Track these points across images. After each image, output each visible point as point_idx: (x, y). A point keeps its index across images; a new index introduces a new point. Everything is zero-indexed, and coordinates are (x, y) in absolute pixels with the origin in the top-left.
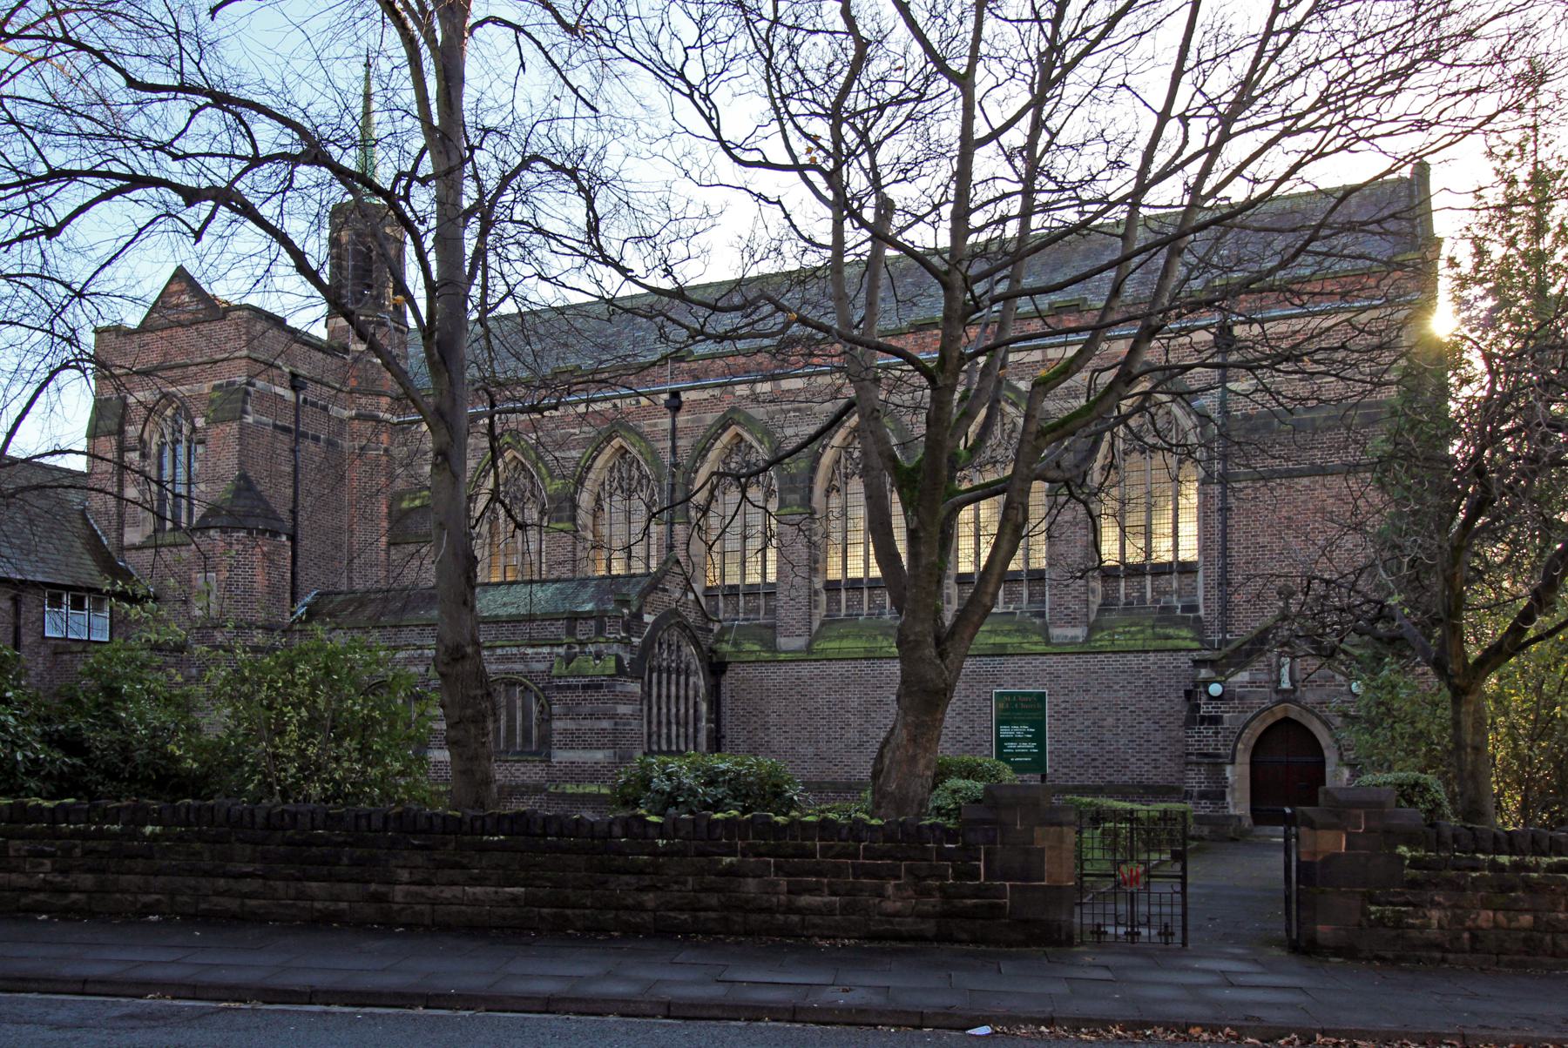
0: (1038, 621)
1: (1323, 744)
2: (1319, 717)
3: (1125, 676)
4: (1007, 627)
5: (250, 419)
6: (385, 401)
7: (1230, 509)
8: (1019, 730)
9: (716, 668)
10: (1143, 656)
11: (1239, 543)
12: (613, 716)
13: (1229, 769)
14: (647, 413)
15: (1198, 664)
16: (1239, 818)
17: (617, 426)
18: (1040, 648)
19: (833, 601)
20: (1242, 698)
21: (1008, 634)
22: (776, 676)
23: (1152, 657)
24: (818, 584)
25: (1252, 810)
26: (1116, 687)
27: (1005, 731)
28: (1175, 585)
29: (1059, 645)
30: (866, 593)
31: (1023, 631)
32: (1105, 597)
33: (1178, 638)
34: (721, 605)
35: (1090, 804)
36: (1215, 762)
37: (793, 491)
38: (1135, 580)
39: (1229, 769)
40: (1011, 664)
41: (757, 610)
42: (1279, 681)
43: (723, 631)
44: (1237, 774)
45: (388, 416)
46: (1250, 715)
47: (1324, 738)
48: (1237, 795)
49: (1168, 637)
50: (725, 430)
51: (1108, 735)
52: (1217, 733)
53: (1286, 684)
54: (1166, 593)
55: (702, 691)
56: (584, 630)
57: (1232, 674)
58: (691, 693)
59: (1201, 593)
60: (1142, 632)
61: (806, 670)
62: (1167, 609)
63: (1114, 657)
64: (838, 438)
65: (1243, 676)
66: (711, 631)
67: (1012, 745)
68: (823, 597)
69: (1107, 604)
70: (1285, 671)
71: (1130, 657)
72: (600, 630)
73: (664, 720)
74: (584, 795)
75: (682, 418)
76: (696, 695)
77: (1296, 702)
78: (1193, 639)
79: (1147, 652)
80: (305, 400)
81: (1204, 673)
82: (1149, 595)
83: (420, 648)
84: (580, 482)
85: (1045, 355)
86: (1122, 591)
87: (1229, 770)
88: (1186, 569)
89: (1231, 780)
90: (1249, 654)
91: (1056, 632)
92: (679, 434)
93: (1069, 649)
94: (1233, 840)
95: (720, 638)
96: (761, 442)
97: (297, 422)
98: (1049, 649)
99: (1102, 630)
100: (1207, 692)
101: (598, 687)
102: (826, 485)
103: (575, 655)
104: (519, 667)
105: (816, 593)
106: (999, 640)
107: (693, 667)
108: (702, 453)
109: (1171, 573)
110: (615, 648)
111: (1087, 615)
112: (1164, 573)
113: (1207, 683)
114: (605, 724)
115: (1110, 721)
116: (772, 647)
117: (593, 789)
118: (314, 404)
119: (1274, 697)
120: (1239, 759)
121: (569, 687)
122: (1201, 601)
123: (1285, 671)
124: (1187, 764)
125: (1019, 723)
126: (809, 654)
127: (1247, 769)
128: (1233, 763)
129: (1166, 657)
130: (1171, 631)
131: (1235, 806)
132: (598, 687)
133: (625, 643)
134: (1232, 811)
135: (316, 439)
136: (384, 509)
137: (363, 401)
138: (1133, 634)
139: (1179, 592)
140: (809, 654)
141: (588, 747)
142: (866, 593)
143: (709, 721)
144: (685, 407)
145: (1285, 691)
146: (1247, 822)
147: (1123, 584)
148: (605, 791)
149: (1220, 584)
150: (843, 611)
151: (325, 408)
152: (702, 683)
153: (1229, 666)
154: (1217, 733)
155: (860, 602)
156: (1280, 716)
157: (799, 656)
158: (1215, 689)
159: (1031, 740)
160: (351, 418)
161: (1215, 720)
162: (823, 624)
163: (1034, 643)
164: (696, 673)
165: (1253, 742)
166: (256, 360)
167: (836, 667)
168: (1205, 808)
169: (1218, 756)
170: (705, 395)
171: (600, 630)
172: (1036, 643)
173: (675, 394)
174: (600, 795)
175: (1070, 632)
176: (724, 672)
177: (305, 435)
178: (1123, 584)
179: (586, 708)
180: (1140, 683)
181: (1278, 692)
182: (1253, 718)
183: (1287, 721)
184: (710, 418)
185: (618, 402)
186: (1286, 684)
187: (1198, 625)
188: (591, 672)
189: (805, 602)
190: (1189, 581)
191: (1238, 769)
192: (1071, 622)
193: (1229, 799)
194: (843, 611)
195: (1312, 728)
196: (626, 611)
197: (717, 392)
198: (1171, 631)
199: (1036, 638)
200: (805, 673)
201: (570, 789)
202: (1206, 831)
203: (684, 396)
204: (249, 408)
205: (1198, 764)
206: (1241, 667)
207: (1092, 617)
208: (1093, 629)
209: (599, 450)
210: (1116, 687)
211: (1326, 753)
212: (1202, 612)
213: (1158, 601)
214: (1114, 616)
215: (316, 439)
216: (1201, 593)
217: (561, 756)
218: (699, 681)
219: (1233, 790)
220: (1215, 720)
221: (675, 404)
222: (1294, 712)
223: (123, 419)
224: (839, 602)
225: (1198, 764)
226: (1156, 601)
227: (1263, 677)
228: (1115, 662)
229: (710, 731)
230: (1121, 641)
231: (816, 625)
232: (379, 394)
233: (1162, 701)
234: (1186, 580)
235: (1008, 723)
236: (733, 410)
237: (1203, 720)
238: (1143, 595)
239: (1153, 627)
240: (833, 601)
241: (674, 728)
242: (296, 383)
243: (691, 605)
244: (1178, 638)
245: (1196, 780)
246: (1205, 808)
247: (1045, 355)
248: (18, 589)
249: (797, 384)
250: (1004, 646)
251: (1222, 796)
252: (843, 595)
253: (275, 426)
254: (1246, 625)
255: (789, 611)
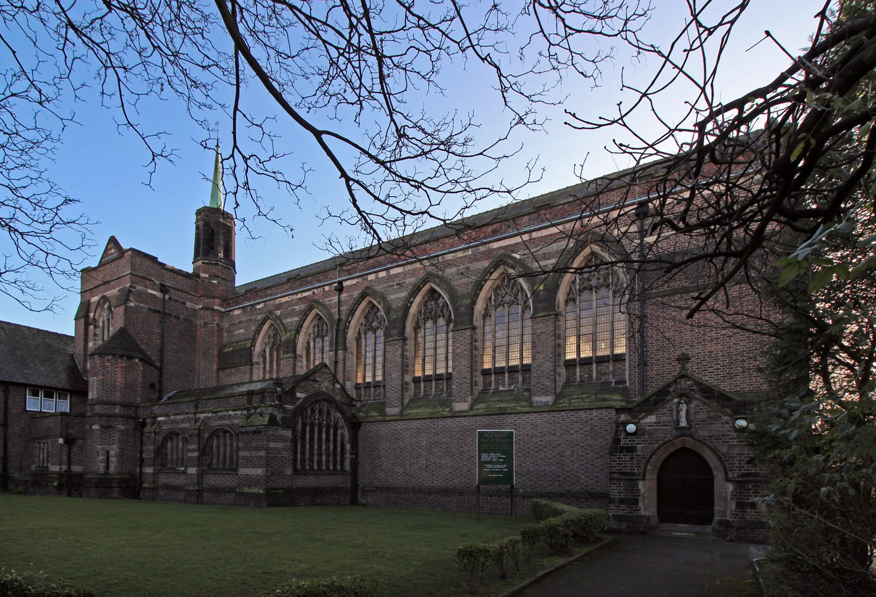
0: (526, 394)
1: (712, 466)
2: (709, 447)
3: (578, 425)
4: (508, 398)
5: (132, 304)
6: (217, 301)
7: (645, 316)
8: (494, 456)
9: (355, 426)
10: (589, 412)
11: (652, 337)
12: (267, 449)
13: (641, 483)
14: (326, 294)
15: (619, 411)
16: (648, 518)
17: (312, 304)
18: (526, 409)
19: (417, 388)
20: (650, 434)
21: (508, 402)
22: (384, 429)
23: (595, 413)
24: (408, 378)
25: (658, 512)
26: (572, 432)
27: (485, 457)
28: (611, 368)
29: (537, 407)
30: (434, 383)
31: (517, 399)
32: (568, 379)
33: (612, 400)
34: (363, 393)
35: (545, 506)
36: (631, 479)
37: (394, 328)
38: (586, 367)
39: (641, 483)
40: (509, 419)
41: (379, 395)
42: (678, 421)
43: (362, 406)
44: (647, 488)
45: (220, 308)
46: (656, 446)
47: (713, 462)
48: (647, 501)
49: (605, 400)
50: (363, 300)
51: (568, 461)
52: (632, 459)
53: (683, 423)
54: (605, 374)
55: (347, 438)
56: (256, 400)
57: (644, 418)
58: (339, 438)
59: (627, 373)
60: (589, 397)
61: (400, 425)
62: (607, 383)
63: (571, 413)
64: (419, 298)
65: (652, 419)
66: (355, 406)
67: (489, 466)
68: (412, 386)
69: (568, 383)
70: (683, 414)
71: (581, 413)
72: (262, 401)
73: (316, 452)
74: (252, 494)
75: (344, 295)
76: (342, 441)
77: (692, 436)
78: (621, 401)
79: (592, 409)
80: (170, 299)
81: (623, 417)
82: (594, 375)
83: (187, 413)
84: (298, 332)
85: (530, 236)
86: (578, 374)
87: (641, 484)
88: (619, 358)
89: (642, 491)
90: (656, 403)
91: (536, 399)
92: (342, 304)
93: (543, 409)
94: (643, 533)
95: (359, 410)
96: (379, 303)
97: (163, 308)
98: (532, 410)
99: (564, 397)
100: (625, 430)
101: (259, 432)
102: (414, 325)
103: (252, 414)
104: (228, 422)
105: (407, 383)
106: (503, 405)
107: (340, 424)
108: (352, 312)
109: (608, 361)
110: (270, 410)
111: (555, 388)
112: (605, 362)
113: (625, 424)
114: (263, 453)
115: (568, 453)
116: (383, 413)
117: (255, 490)
118: (175, 301)
119: (674, 432)
120: (648, 476)
121: (247, 433)
122: (627, 376)
123: (683, 414)
124: (611, 480)
125: (495, 452)
126: (402, 417)
127: (654, 484)
128: (644, 479)
129: (604, 412)
130: (607, 396)
131: (645, 509)
132: (259, 432)
133: (281, 407)
134: (643, 513)
135: (178, 318)
136: (216, 352)
137: (206, 301)
138: (583, 399)
139: (613, 373)
140: (402, 417)
141: (255, 466)
142: (434, 383)
143: (351, 454)
144: (345, 289)
145: (683, 428)
146: (654, 521)
147: (578, 370)
148: (261, 491)
149: (639, 365)
150: (422, 393)
151: (185, 304)
152: (346, 433)
153: (641, 412)
154: (632, 459)
155: (431, 389)
156: (679, 446)
157: (396, 418)
158: (631, 428)
159: (503, 463)
160: (200, 309)
161: (631, 450)
162: (411, 401)
163: (523, 407)
164: (342, 428)
165: (659, 464)
166: (136, 276)
167: (415, 424)
168: (623, 510)
169: (634, 474)
170: (354, 281)
171: (262, 401)
172: (524, 407)
173: (340, 283)
174: (258, 494)
175: (544, 399)
176: (359, 427)
177: (170, 315)
178: (578, 370)
179: (254, 444)
180: (587, 429)
181: (677, 429)
182: (659, 448)
183: (684, 449)
184: (356, 294)
185: (315, 290)
186: (683, 423)
187: (625, 392)
188: (257, 423)
189: (400, 388)
190: (620, 366)
191: (648, 483)
192: (545, 393)
193: (641, 504)
194: (422, 393)
195: (704, 455)
196: (279, 389)
197: (360, 280)
198: (607, 396)
199: (524, 404)
200: (399, 427)
201: (246, 490)
202: (624, 526)
203: (345, 284)
204: (131, 298)
205: (619, 480)
206: (649, 412)
207: (559, 390)
208: (558, 397)
209: (306, 316)
210: (572, 432)
211: (715, 473)
212: (628, 384)
213: (601, 379)
214: (572, 389)
215: (178, 318)
216: (627, 373)
217: (243, 471)
218: (345, 432)
219: (644, 498)
220: (631, 450)
221: (340, 289)
222: (690, 443)
223: (88, 311)
224: (420, 389)
225: (619, 480)
226: (598, 379)
227: (666, 418)
228: (572, 416)
229: (352, 459)
230: (575, 403)
231: (406, 401)
232: (214, 298)
233: (600, 440)
234: (618, 365)
235: (488, 452)
236: (367, 288)
237: (622, 449)
238: (591, 376)
239: (596, 394)
240: (417, 388)
241: (324, 457)
242: (163, 289)
243: (337, 391)
244: (612, 400)
245: (617, 491)
246: (623, 510)
247: (530, 236)
248: (7, 385)
249: (399, 270)
250: (505, 408)
251: (636, 502)
252: (422, 384)
253: (149, 309)
254: (653, 387)
255: (392, 394)
